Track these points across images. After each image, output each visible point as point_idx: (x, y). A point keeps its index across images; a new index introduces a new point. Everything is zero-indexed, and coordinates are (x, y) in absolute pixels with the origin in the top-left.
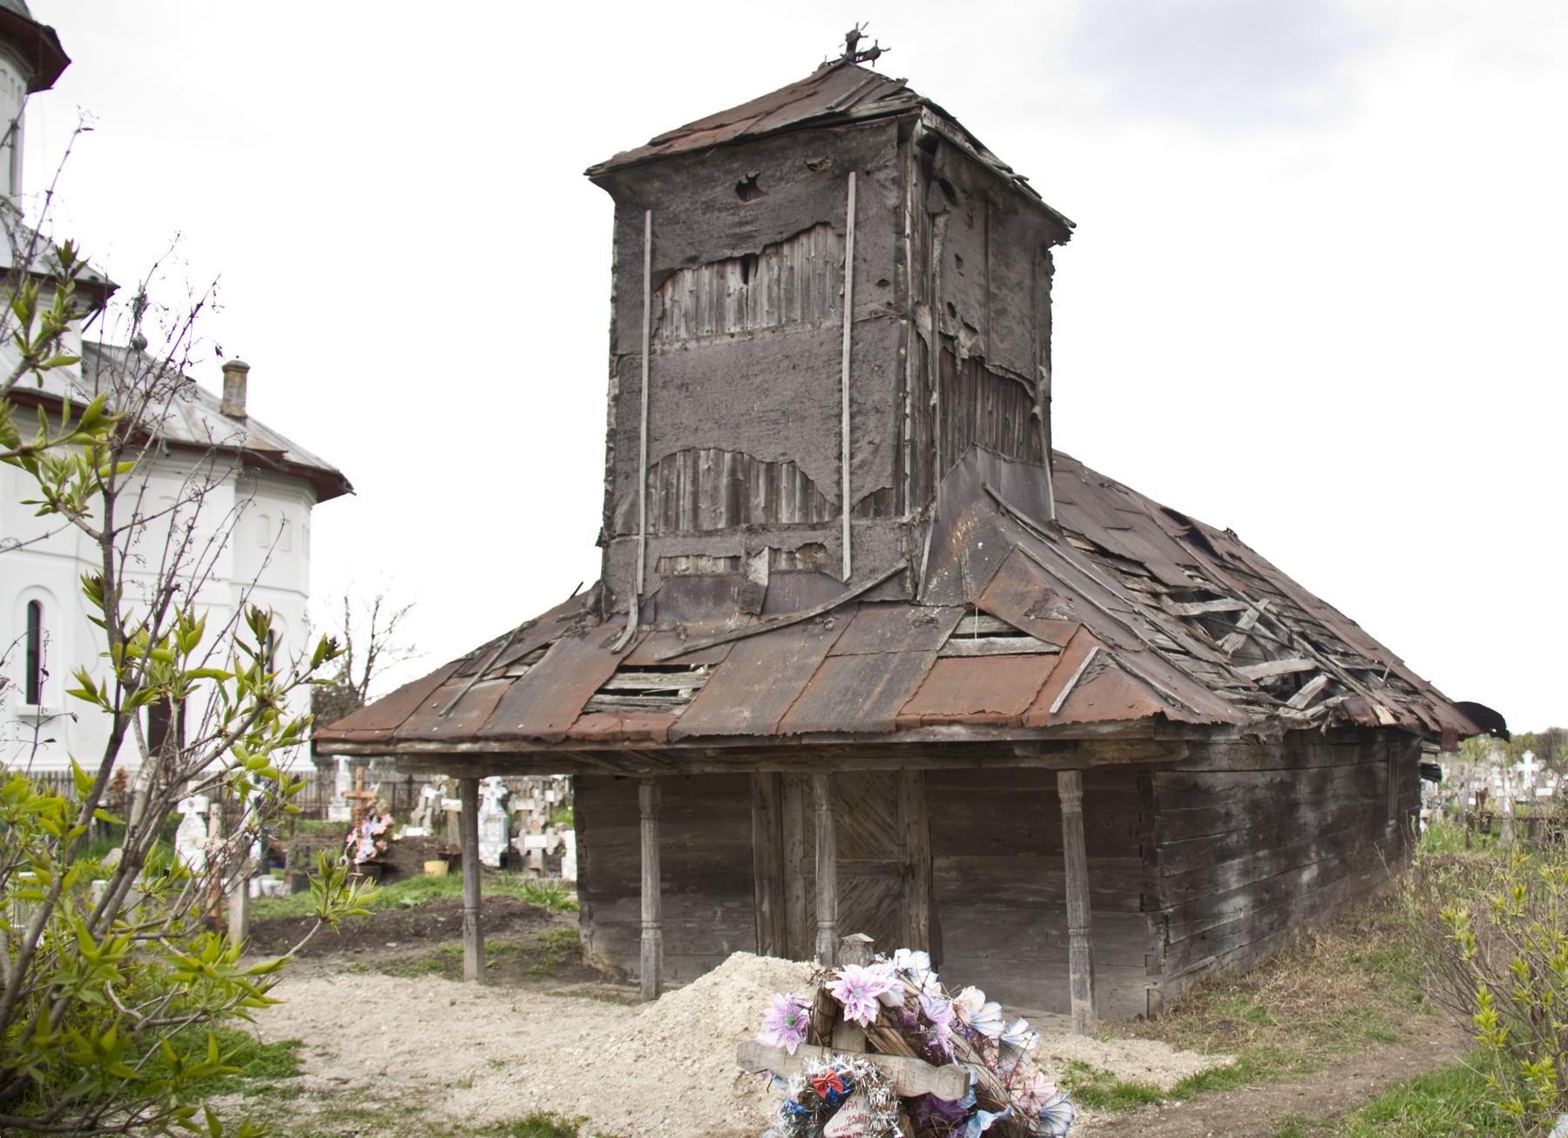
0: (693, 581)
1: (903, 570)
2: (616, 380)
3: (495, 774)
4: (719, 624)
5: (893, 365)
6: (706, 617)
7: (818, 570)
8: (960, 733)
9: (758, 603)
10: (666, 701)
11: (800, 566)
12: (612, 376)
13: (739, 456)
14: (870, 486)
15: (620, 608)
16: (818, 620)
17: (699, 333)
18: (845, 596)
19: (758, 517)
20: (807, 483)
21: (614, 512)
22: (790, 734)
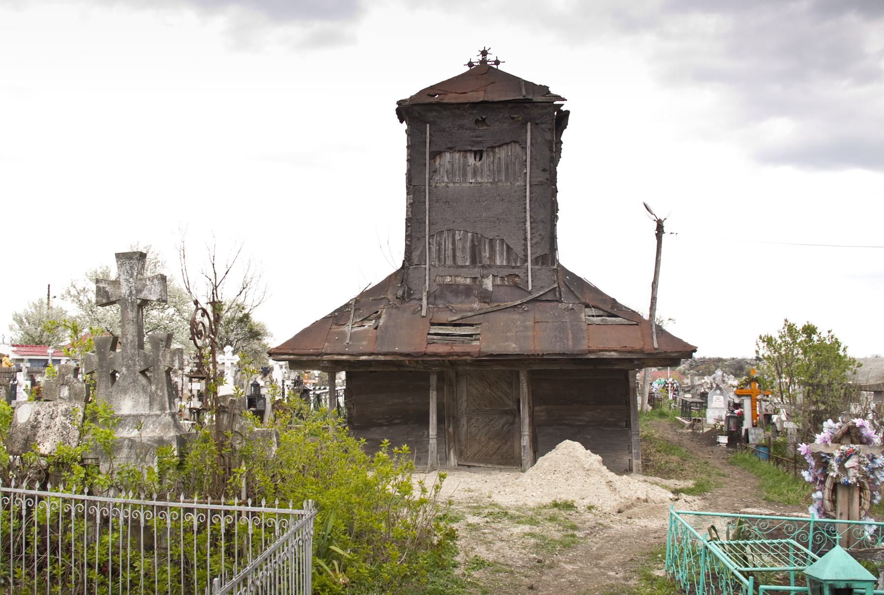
0: (454, 287)
1: (556, 288)
2: (411, 196)
3: (318, 369)
4: (470, 306)
5: (550, 204)
6: (462, 302)
7: (516, 286)
8: (614, 355)
9: (485, 297)
10: (465, 339)
11: (506, 283)
12: (408, 194)
13: (475, 235)
14: (540, 252)
15: (417, 296)
16: (519, 306)
17: (454, 180)
18: (530, 298)
19: (486, 261)
20: (509, 249)
21: (411, 254)
22: (541, 354)
